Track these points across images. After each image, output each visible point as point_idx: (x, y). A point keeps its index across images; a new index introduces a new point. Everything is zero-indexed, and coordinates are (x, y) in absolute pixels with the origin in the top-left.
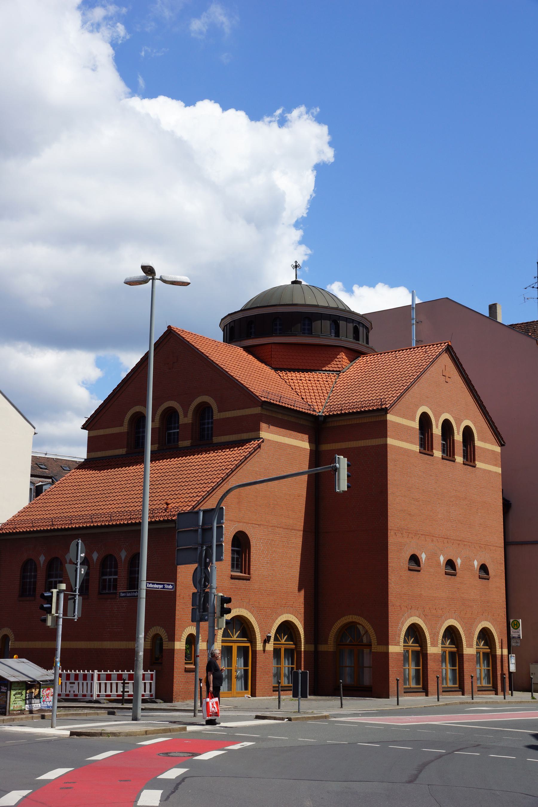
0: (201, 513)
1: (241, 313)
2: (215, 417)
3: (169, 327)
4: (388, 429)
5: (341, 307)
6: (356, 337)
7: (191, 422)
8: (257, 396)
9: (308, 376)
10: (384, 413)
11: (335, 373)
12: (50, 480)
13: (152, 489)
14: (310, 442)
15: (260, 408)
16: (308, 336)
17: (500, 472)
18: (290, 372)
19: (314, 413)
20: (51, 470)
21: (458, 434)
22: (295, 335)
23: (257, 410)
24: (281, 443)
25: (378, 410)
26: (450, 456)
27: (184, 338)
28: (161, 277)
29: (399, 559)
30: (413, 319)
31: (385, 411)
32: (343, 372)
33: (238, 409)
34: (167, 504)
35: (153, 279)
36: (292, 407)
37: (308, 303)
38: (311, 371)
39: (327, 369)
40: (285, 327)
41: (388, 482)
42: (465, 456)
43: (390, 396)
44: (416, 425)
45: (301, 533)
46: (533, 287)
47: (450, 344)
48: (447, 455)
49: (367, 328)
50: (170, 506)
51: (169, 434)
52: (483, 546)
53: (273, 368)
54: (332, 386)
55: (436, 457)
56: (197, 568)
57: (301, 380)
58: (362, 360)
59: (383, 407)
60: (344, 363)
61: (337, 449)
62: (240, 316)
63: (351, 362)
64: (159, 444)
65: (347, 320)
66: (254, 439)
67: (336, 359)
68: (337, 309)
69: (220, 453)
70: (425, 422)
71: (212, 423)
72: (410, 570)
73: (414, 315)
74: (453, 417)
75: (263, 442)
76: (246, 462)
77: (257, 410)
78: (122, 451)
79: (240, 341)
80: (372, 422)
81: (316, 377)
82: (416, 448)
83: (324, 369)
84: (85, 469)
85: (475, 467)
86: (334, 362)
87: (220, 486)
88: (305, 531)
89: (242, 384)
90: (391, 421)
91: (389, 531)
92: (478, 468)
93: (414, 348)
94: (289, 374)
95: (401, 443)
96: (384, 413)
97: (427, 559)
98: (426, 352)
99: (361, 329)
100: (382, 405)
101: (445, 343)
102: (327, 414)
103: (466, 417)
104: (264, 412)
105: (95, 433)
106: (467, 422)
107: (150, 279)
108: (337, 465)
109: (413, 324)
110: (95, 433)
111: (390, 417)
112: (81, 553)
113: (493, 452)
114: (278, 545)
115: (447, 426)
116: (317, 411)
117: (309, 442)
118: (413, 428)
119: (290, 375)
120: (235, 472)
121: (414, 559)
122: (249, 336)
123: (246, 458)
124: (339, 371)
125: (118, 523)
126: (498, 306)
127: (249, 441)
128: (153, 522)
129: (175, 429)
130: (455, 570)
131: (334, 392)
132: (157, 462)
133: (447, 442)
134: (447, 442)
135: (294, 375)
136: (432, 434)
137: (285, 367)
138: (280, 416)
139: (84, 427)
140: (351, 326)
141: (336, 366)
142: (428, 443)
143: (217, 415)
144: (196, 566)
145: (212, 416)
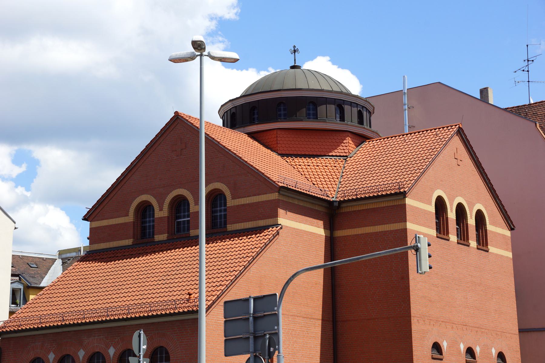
0: (252, 301)
1: (243, 99)
2: (229, 204)
3: (176, 113)
4: (407, 213)
5: (344, 91)
6: (361, 122)
7: (132, 220)
8: (274, 182)
9: (315, 162)
10: (402, 197)
11: (342, 158)
12: (18, 278)
13: (146, 283)
14: (325, 228)
15: (277, 194)
16: (314, 121)
17: (511, 257)
18: (287, 157)
19: (329, 199)
20: (17, 267)
21: (471, 218)
22: (301, 120)
23: (274, 196)
24: (298, 229)
25: (396, 194)
26: (464, 240)
27: (192, 124)
28: (209, 53)
29: (422, 347)
30: (405, 104)
31: (404, 195)
32: (351, 157)
33: (253, 196)
34: (190, 294)
35: (201, 55)
36: (308, 193)
37: (311, 87)
38: (318, 156)
39: (334, 154)
40: (280, 112)
41: (410, 267)
42: (478, 241)
43: (406, 180)
44: (432, 209)
45: (320, 322)
46: (523, 70)
47: (461, 126)
48: (461, 239)
49: (370, 112)
50: (192, 296)
51: (179, 223)
52: (499, 333)
53: (279, 154)
54: (341, 171)
55: (452, 241)
56: (249, 358)
57: (309, 166)
58: (367, 146)
59: (402, 190)
60: (350, 148)
61: (353, 235)
62: (243, 101)
63: (357, 147)
64: (134, 238)
65: (351, 104)
66: (272, 226)
67: (343, 144)
68: (341, 93)
69: (237, 241)
70: (440, 204)
71: (225, 210)
72: (433, 358)
73: (405, 100)
74: (466, 200)
75: (281, 228)
76: (266, 249)
77: (274, 196)
78: (128, 242)
79: (244, 127)
80: (391, 205)
81: (324, 162)
82: (433, 232)
83: (330, 154)
84: (89, 261)
85: (487, 251)
86: (341, 147)
87: (242, 275)
88: (323, 320)
89: (258, 170)
90: (409, 205)
91: (412, 318)
92: (491, 253)
93: (407, 135)
94: (296, 160)
95: (420, 227)
96: (402, 197)
97: (449, 347)
98: (437, 134)
99: (365, 113)
100: (399, 189)
101: (456, 126)
102: (342, 199)
103: (478, 202)
104: (281, 198)
105: (97, 224)
106: (479, 206)
107: (197, 56)
108: (419, 244)
109: (405, 110)
110: (97, 224)
111: (409, 201)
112: (143, 345)
113: (504, 236)
114: (298, 335)
115: (461, 210)
116: (331, 196)
117: (324, 228)
118: (430, 212)
119: (297, 161)
120: (256, 260)
121: (437, 347)
122: (252, 122)
123: (266, 245)
124: (346, 156)
125: (55, 324)
126: (489, 90)
127: (267, 227)
128: (177, 313)
129: (184, 217)
130: (475, 358)
131: (344, 177)
132: (169, 251)
133: (460, 227)
134: (460, 227)
135: (302, 161)
136: (447, 218)
137: (291, 153)
138: (296, 202)
139: (85, 218)
140: (355, 110)
141: (343, 151)
142: (444, 228)
143: (231, 202)
144: (248, 356)
145: (154, 214)
